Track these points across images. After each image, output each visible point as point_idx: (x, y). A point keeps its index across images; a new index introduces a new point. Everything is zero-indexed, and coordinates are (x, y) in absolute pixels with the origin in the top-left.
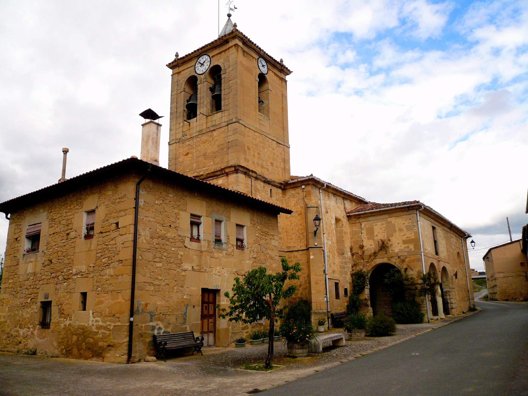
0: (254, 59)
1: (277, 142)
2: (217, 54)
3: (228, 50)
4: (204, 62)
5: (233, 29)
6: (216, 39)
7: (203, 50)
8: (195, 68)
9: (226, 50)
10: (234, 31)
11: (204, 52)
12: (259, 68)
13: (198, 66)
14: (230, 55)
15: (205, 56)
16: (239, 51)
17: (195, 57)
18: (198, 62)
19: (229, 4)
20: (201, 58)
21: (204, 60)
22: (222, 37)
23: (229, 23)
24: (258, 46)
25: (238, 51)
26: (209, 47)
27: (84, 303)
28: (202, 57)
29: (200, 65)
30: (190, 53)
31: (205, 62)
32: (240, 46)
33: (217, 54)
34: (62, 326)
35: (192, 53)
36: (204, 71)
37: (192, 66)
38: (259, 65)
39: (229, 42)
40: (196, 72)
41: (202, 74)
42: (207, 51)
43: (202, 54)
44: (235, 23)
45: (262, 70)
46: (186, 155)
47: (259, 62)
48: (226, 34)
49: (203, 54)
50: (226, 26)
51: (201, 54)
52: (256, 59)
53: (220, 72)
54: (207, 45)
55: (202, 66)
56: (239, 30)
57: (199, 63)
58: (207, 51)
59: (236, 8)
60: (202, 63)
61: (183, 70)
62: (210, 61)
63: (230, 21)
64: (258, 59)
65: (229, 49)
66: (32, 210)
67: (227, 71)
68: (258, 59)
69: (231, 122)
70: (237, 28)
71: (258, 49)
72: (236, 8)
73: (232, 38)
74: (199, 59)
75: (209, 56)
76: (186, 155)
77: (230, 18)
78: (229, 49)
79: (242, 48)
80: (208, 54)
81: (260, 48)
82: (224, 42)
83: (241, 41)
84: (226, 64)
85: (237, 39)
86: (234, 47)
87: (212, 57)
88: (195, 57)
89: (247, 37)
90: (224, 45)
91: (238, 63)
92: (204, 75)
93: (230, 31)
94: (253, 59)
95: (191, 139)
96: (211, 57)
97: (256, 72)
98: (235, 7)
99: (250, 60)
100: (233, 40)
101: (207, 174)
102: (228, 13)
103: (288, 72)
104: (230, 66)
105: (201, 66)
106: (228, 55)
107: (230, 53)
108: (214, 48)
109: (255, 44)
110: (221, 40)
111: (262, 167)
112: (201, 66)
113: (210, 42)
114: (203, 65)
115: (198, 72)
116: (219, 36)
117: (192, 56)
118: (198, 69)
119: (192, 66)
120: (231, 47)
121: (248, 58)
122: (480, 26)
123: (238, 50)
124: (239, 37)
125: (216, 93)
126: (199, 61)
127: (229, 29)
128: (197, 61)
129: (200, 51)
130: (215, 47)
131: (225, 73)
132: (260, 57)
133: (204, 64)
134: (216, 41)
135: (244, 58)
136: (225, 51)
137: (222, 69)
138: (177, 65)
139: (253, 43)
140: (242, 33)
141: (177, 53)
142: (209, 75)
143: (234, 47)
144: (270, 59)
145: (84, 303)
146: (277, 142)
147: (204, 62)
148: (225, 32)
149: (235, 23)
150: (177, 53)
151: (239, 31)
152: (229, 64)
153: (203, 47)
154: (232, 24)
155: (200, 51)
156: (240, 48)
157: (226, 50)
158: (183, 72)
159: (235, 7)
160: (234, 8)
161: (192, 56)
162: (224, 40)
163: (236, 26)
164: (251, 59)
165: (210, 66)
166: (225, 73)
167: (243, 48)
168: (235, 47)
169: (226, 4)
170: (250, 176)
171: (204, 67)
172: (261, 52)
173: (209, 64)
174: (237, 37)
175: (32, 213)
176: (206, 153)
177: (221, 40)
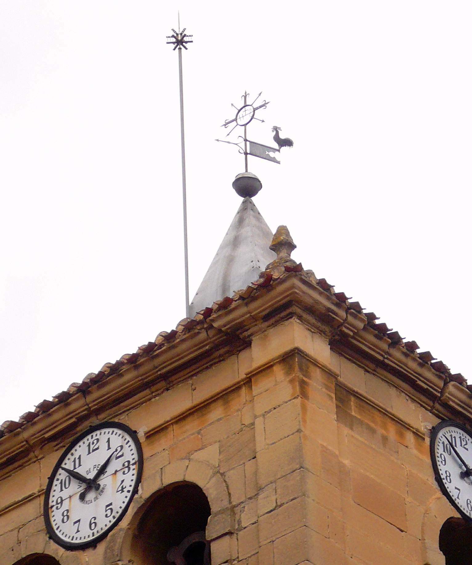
0: (410, 437)
2: (3, 479)
3: (244, 390)
4: (102, 470)
5: (273, 266)
6: (170, 326)
7: (96, 394)
8: (47, 509)
9: (235, 389)
10: (276, 275)
11: (98, 412)
12: (445, 492)
13: (65, 494)
14: (259, 422)
15: (104, 435)
16: (311, 392)
17: (44, 442)
18: (62, 475)
19: (241, 122)
20: (81, 449)
21: (100, 458)
22: (208, 312)
23: (246, 231)
24: (427, 356)
25: (304, 394)
27: (436, 517)
28: (88, 439)
29: (75, 488)
30: (17, 419)
31: (110, 470)
32: (315, 363)
33: (181, 418)
35: (29, 418)
36: (104, 523)
37: (29, 499)
38: (442, 469)
39: (247, 344)
40: (52, 536)
41: (92, 544)
42: (117, 401)
43: (86, 424)
44: (283, 230)
45: (461, 503)
47: (439, 450)
48: (231, 295)
49: (94, 421)
50: (227, 251)
51: (81, 420)
52: (417, 434)
53: (202, 525)
54: (119, 364)
55: (91, 496)
56: (305, 268)
57: (74, 475)
58: (117, 401)
59: (288, 143)
60: (84, 486)
62: (141, 463)
63: (250, 219)
64: (434, 432)
65: (249, 381)
67: (246, 519)
68: (434, 432)
70: (296, 256)
71: (429, 374)
72: (288, 143)
73: (266, 318)
75: (133, 434)
77: (254, 199)
78: (249, 381)
79: (329, 373)
80: (122, 419)
81: (440, 368)
82: (216, 347)
83: (322, 332)
84: (233, 476)
85: (295, 321)
86: (279, 371)
87: (152, 435)
88: (44, 442)
89: (356, 307)
90: (221, 359)
91: (307, 465)
92: (101, 547)
93: (255, 279)
94: (401, 435)
96: (141, 435)
97: (426, 512)
98: (282, 136)
99: (385, 439)
100: (271, 331)
102: (241, 170)
104: (260, 489)
105: (82, 497)
106: (247, 421)
107: (261, 406)
108: (163, 384)
109: (412, 346)
110: (203, 335)
112: (82, 497)
113: (134, 350)
114: (98, 487)
116: (190, 308)
117: (25, 435)
118: (66, 516)
119: (29, 499)
120: (266, 368)
121: (373, 431)
122: (346, 304)
123: (303, 384)
124: (310, 310)
126: (68, 464)
127: (245, 269)
128: (58, 466)
129: (77, 405)
130: (165, 377)
131: (230, 533)
132: (444, 422)
133: (104, 481)
134: (169, 337)
135: (346, 431)
137: (214, 507)
139: (395, 339)
140: (323, 283)
142: (133, 546)
143: (279, 371)
145: (436, 517)
147: (102, 470)
148: (225, 287)
149: (283, 230)
151: (310, 273)
152: (256, 473)
154: (268, 232)
155: (73, 407)
156: (317, 374)
157: (235, 389)
159: (277, 138)
160: (276, 146)
161: (25, 435)
162: (219, 331)
163: (292, 247)
164: (392, 431)
165: (135, 491)
166: (230, 533)
167: (335, 369)
168: (289, 370)
169: (226, 125)
171: (104, 500)
172: (451, 387)
173: (130, 478)
174: (295, 309)
177: (203, 335)
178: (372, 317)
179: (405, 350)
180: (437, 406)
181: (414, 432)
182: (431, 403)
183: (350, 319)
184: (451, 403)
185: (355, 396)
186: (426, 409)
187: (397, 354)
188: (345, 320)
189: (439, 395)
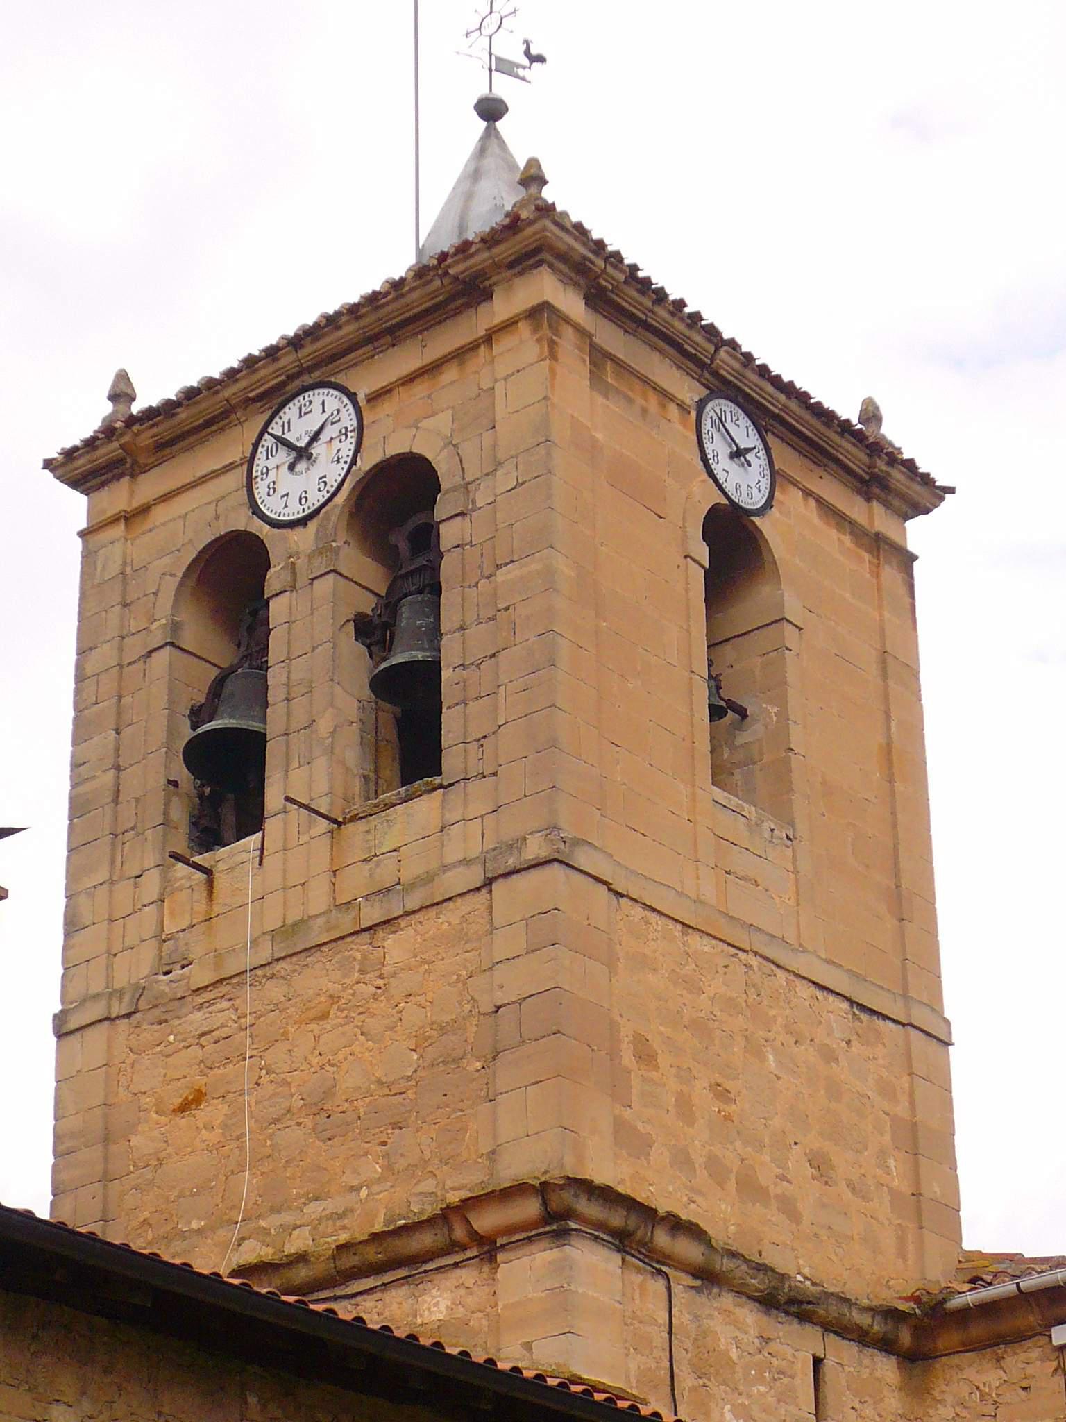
1: (852, 1002)
26: (349, 330)
46: (183, 1108)
49: (307, 379)
69: (512, 862)
103: (916, 490)
111: (750, 1188)
138: (121, 461)
144: (785, 408)
146: (852, 1002)
160: (526, 62)
161: (227, 393)
170: (656, 1262)
176: (329, 1093)
178: (634, 268)
179: (671, 308)
180: (706, 374)
181: (678, 404)
182: (699, 371)
183: (610, 270)
184: (722, 372)
185: (612, 360)
186: (694, 378)
187: (661, 312)
188: (604, 271)
189: (709, 362)
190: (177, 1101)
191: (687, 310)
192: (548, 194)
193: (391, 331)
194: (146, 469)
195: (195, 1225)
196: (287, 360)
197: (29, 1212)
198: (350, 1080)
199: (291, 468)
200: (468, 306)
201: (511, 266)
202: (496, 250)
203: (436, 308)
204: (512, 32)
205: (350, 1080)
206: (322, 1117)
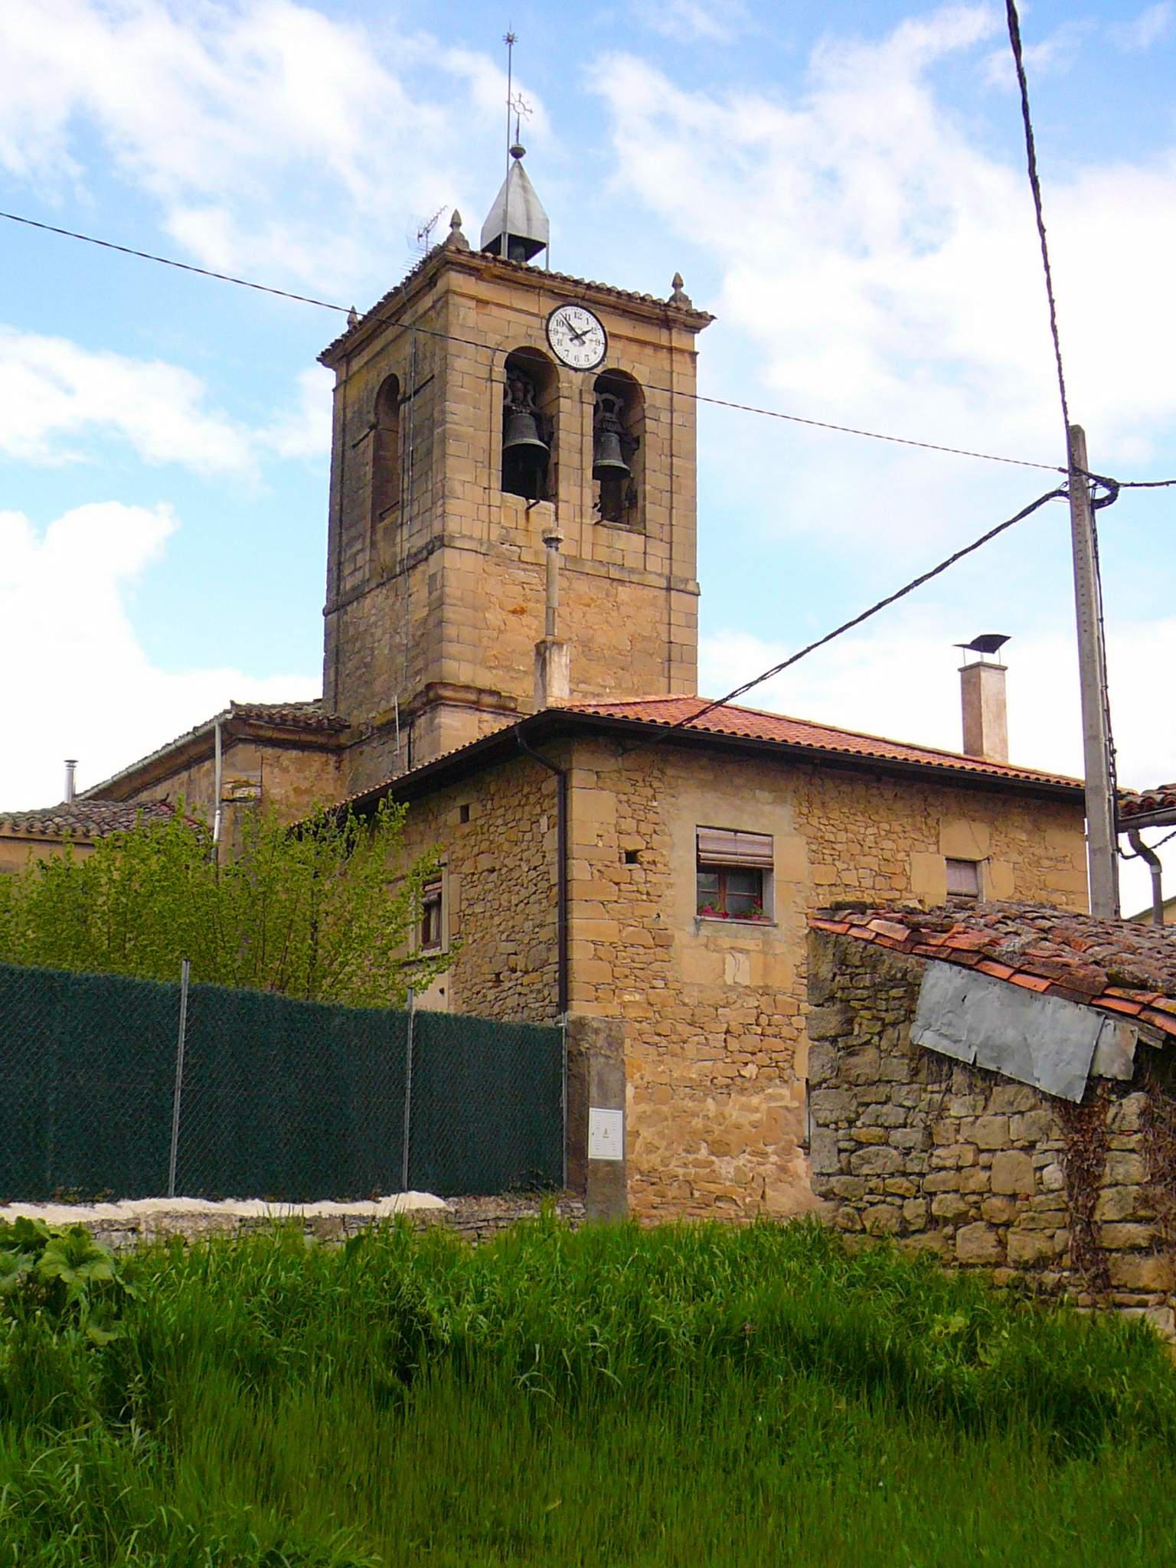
26: (612, 299)
34: (266, 1300)
46: (514, 612)
49: (585, 304)
60: (579, 332)
61: (498, 305)
66: (710, 777)
69: (682, 587)
74: (563, 306)
76: (514, 612)
95: (537, 568)
101: (832, 768)
115: (595, 359)
125: (606, 462)
136: (643, 343)
138: (478, 270)
141: (677, 277)
150: (677, 277)
153: (599, 289)
155: (578, 289)
158: (495, 311)
161: (546, 282)
162: (667, 316)
175: (702, 785)
176: (591, 640)
190: (512, 609)
191: (537, 261)
192: (683, 290)
193: (624, 311)
194: (483, 280)
195: (521, 668)
196: (581, 290)
197: (982, 637)
198: (601, 639)
199: (571, 340)
200: (657, 325)
201: (686, 326)
202: (689, 319)
203: (650, 318)
204: (510, 40)
205: (601, 639)
206: (586, 649)
